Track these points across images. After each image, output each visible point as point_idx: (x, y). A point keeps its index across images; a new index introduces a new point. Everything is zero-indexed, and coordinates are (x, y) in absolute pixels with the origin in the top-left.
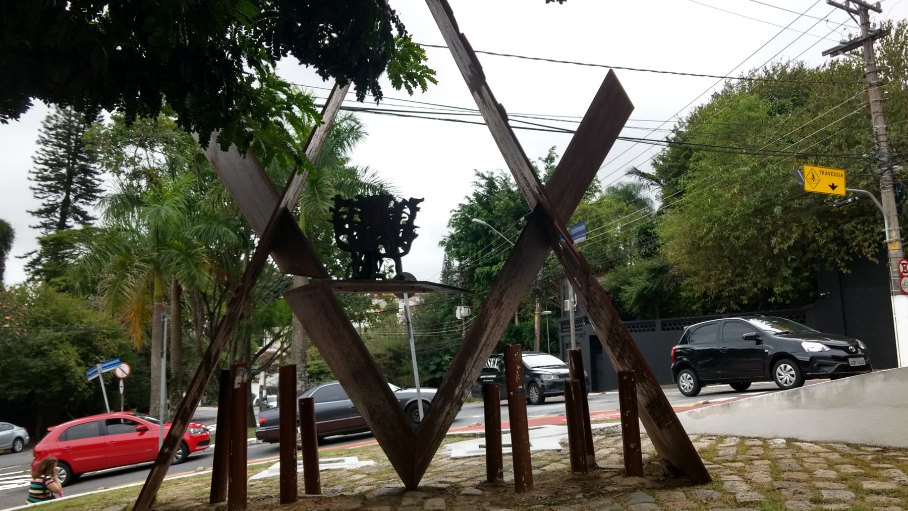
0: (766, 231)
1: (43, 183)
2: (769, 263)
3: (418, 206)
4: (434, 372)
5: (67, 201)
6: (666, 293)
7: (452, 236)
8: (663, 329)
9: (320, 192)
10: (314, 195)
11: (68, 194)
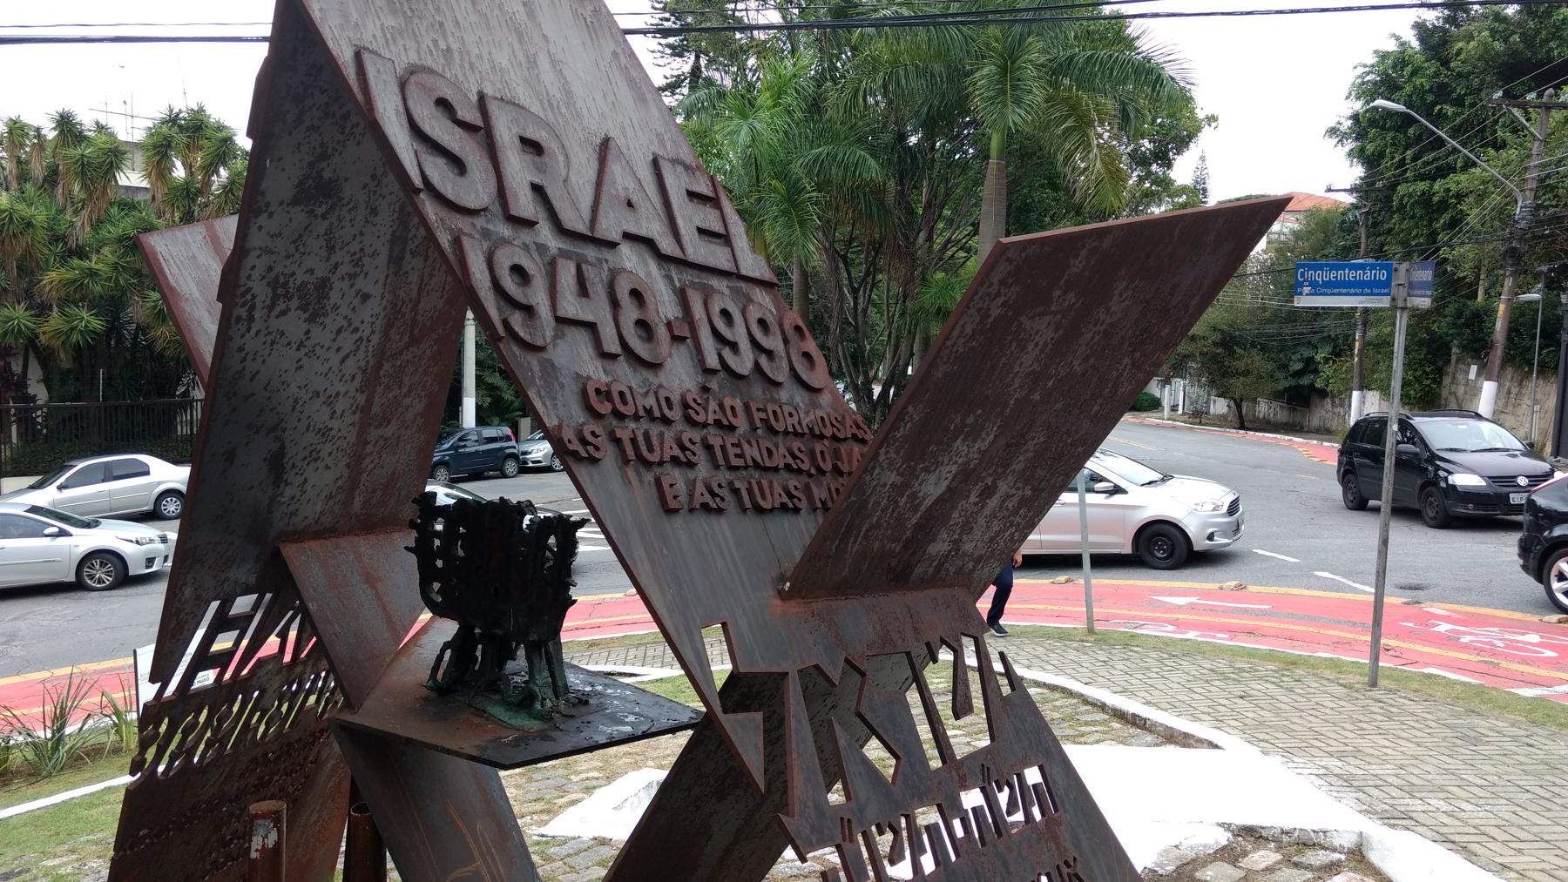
1: (663, 41)
4: (1298, 374)
5: (696, 71)
7: (1355, 117)
9: (1014, 88)
10: (1004, 92)
11: (698, 58)
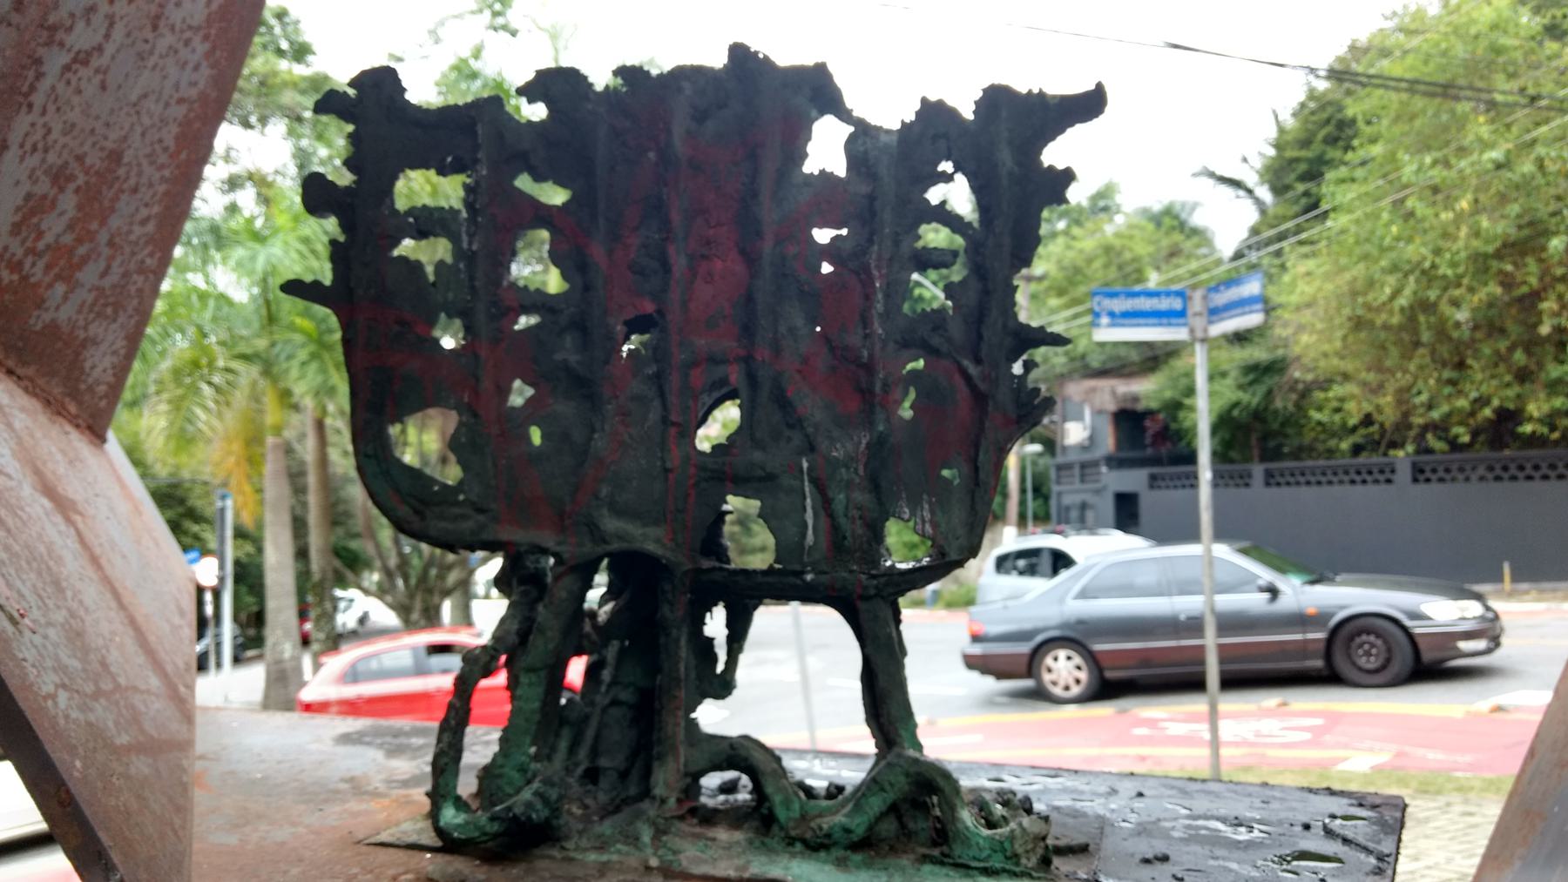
0: (1525, 289)
2: (1519, 357)
3: (1054, 155)
6: (1276, 412)
8: (1268, 484)
